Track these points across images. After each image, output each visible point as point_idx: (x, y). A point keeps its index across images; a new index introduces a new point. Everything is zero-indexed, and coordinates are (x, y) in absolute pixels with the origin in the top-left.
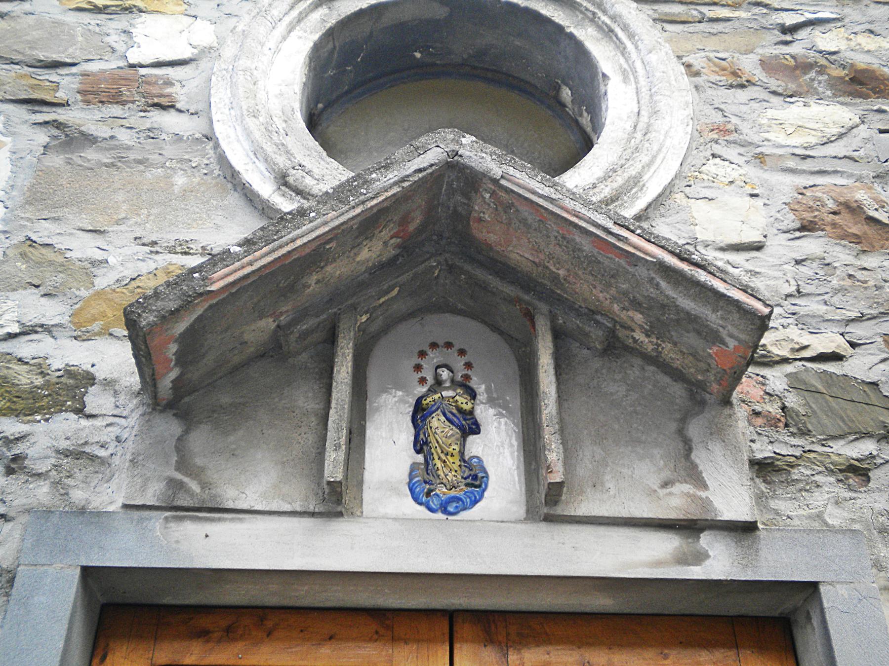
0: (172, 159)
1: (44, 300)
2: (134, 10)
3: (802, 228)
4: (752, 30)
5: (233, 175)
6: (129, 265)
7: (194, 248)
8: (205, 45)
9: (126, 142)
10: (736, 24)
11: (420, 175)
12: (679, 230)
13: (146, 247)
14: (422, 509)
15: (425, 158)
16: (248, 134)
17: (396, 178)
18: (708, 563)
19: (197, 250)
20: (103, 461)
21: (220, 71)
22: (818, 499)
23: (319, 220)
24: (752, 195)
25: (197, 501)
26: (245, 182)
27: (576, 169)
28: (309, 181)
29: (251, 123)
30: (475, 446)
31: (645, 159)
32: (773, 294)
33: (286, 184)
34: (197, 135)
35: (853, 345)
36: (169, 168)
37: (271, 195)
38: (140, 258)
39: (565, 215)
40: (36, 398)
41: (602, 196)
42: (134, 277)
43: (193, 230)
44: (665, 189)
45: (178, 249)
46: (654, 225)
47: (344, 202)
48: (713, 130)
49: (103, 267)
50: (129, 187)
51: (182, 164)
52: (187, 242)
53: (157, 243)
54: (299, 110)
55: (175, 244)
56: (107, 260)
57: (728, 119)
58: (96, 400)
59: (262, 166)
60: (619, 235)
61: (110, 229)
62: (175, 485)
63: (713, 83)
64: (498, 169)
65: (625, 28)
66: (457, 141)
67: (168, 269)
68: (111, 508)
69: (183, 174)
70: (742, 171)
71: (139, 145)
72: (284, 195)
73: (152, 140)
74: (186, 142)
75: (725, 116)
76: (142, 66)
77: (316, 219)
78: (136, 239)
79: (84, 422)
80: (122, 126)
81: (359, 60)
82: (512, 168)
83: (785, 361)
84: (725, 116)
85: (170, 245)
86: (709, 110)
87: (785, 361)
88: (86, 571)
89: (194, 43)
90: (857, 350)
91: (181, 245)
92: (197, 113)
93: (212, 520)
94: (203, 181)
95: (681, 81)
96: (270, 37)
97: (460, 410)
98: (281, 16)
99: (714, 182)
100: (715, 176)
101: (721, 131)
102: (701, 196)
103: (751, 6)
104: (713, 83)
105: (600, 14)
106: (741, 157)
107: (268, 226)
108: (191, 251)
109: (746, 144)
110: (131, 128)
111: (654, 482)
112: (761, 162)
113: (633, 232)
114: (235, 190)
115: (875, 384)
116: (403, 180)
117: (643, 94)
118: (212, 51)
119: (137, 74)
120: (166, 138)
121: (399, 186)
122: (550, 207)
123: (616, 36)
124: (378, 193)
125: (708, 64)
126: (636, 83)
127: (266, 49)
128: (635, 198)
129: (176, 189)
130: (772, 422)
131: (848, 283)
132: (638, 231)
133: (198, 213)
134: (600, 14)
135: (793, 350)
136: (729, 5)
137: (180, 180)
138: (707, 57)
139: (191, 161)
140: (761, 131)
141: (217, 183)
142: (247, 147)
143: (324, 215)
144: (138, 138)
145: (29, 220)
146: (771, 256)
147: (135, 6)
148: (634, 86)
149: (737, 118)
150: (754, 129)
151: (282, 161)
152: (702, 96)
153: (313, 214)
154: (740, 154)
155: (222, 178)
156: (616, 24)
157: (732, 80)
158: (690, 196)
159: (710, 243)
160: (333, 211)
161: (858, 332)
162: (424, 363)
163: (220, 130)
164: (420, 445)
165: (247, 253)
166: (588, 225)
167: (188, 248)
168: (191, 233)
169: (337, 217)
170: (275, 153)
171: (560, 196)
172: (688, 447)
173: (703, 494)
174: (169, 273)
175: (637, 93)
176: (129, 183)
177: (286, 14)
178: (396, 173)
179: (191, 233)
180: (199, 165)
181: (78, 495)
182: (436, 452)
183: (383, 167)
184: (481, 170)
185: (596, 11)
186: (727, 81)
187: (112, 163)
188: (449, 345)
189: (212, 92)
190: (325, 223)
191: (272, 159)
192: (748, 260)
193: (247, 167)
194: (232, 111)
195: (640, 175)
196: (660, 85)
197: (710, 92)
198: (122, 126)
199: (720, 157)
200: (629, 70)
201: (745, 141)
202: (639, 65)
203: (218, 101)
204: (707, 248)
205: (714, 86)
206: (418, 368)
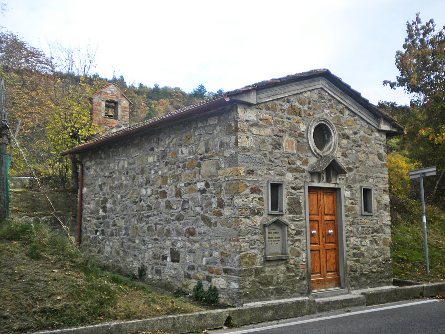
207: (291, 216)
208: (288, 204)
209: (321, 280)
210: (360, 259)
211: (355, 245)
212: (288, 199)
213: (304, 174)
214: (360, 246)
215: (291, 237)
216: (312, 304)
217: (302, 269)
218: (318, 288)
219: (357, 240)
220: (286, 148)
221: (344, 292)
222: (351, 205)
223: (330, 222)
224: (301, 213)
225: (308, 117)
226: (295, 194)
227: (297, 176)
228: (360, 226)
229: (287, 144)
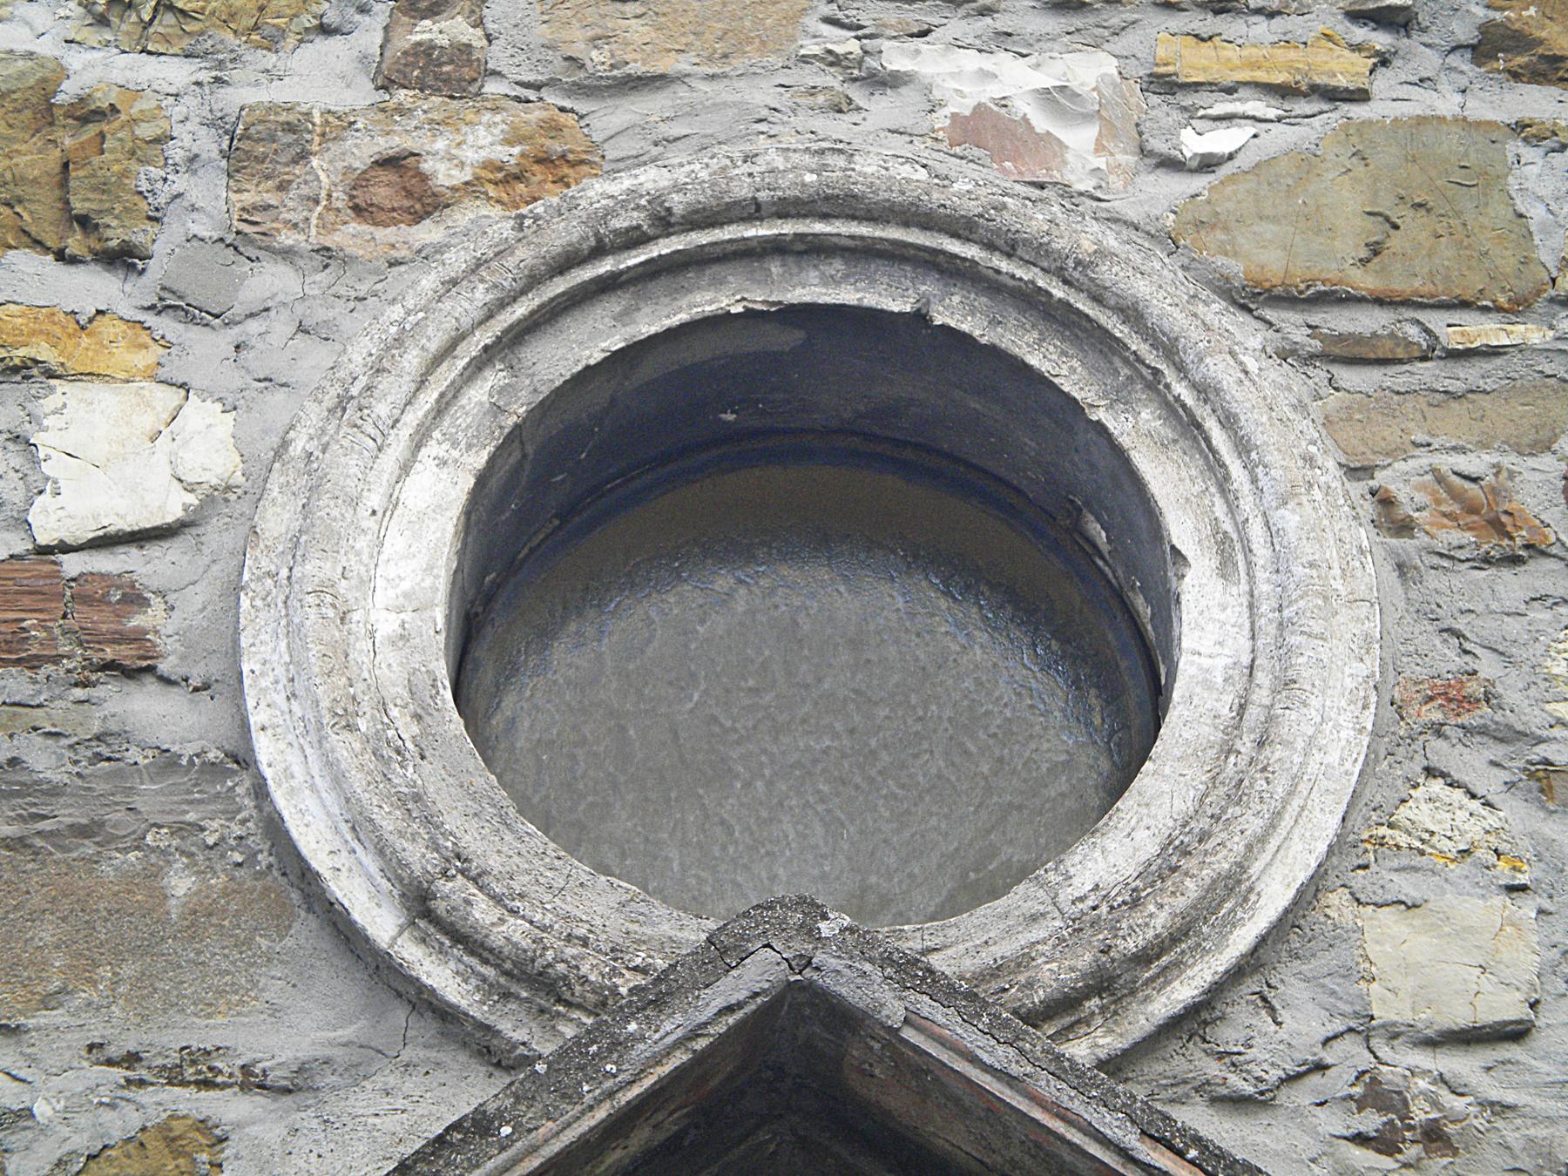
0: (160, 827)
2: (35, 371)
4: (1552, 381)
5: (303, 874)
6: (82, 1120)
7: (226, 1070)
8: (214, 481)
9: (48, 774)
10: (1516, 362)
11: (731, 1021)
12: (1333, 993)
13: (115, 1070)
15: (740, 977)
16: (338, 780)
17: (679, 1033)
19: (231, 1075)
21: (259, 579)
23: (519, 1144)
24: (1512, 889)
26: (333, 900)
27: (1097, 839)
28: (483, 912)
29: (344, 747)
31: (1254, 825)
32: (1540, 1161)
33: (429, 915)
34: (213, 755)
36: (153, 850)
37: (394, 939)
38: (104, 1100)
39: (1037, 1114)
41: (1150, 934)
42: (94, 1151)
43: (219, 1019)
44: (1301, 893)
46: (1273, 982)
47: (570, 1097)
48: (1431, 699)
49: (25, 1128)
50: (65, 905)
51: (183, 838)
52: (209, 1053)
53: (140, 1059)
54: (447, 684)
55: (182, 1059)
56: (30, 1110)
57: (1473, 664)
59: (371, 864)
60: (1150, 1165)
61: (31, 1022)
63: (1441, 555)
64: (896, 1003)
65: (1229, 422)
66: (810, 932)
67: (171, 1130)
69: (187, 866)
70: (1492, 820)
71: (79, 782)
72: (424, 941)
73: (106, 764)
74: (188, 772)
75: (1466, 652)
76: (65, 548)
77: (514, 1141)
78: (91, 1047)
80: (35, 729)
81: (583, 455)
82: (926, 998)
84: (1466, 652)
85: (169, 1062)
86: (1426, 637)
89: (190, 478)
91: (194, 1063)
92: (206, 687)
94: (233, 885)
95: (1359, 573)
96: (371, 477)
98: (397, 412)
99: (1422, 853)
100: (1426, 836)
101: (1450, 700)
102: (1390, 898)
103: (1557, 308)
104: (1441, 555)
105: (1170, 375)
106: (1496, 770)
107: (415, 1162)
108: (219, 1079)
109: (1509, 735)
110: (56, 735)
112: (1542, 791)
113: (1180, 1154)
114: (310, 910)
116: (694, 1035)
117: (1263, 621)
118: (233, 497)
119: (56, 575)
120: (140, 760)
121: (687, 1049)
122: (1007, 1095)
123: (1208, 440)
124: (642, 1071)
125: (1433, 493)
126: (1251, 577)
127: (364, 512)
128: (1232, 923)
132: (1193, 1153)
133: (228, 973)
134: (1170, 375)
136: (1499, 309)
137: (181, 884)
138: (1434, 471)
139: (203, 829)
140: (1548, 696)
141: (267, 889)
142: (336, 810)
143: (530, 1131)
144: (76, 762)
146: (1546, 1057)
147: (36, 362)
148: (1244, 587)
149: (1495, 656)
150: (1533, 691)
151: (418, 857)
152: (1413, 595)
153: (506, 1130)
154: (1494, 764)
155: (276, 873)
156: (1208, 407)
157: (1492, 545)
158: (1363, 899)
159: (1403, 1028)
160: (549, 1119)
163: (265, 749)
166: (1087, 1139)
167: (211, 1069)
168: (215, 1027)
169: (558, 1133)
170: (401, 834)
171: (1029, 1069)
174: (174, 1140)
175: (1251, 606)
176: (66, 896)
177: (409, 403)
178: (678, 1017)
179: (215, 1027)
180: (223, 839)
183: (652, 1002)
184: (861, 1005)
185: (1162, 366)
186: (1478, 547)
187: (21, 839)
189: (244, 642)
190: (533, 1150)
191: (394, 852)
192: (1489, 1069)
193: (339, 861)
194: (295, 705)
195: (1242, 867)
196: (1301, 603)
197: (1433, 581)
198: (35, 729)
199: (1443, 775)
200: (1235, 536)
201: (1509, 727)
202: (1256, 531)
203: (257, 668)
204: (1395, 1042)
205: (1445, 563)
225: (351, 235)
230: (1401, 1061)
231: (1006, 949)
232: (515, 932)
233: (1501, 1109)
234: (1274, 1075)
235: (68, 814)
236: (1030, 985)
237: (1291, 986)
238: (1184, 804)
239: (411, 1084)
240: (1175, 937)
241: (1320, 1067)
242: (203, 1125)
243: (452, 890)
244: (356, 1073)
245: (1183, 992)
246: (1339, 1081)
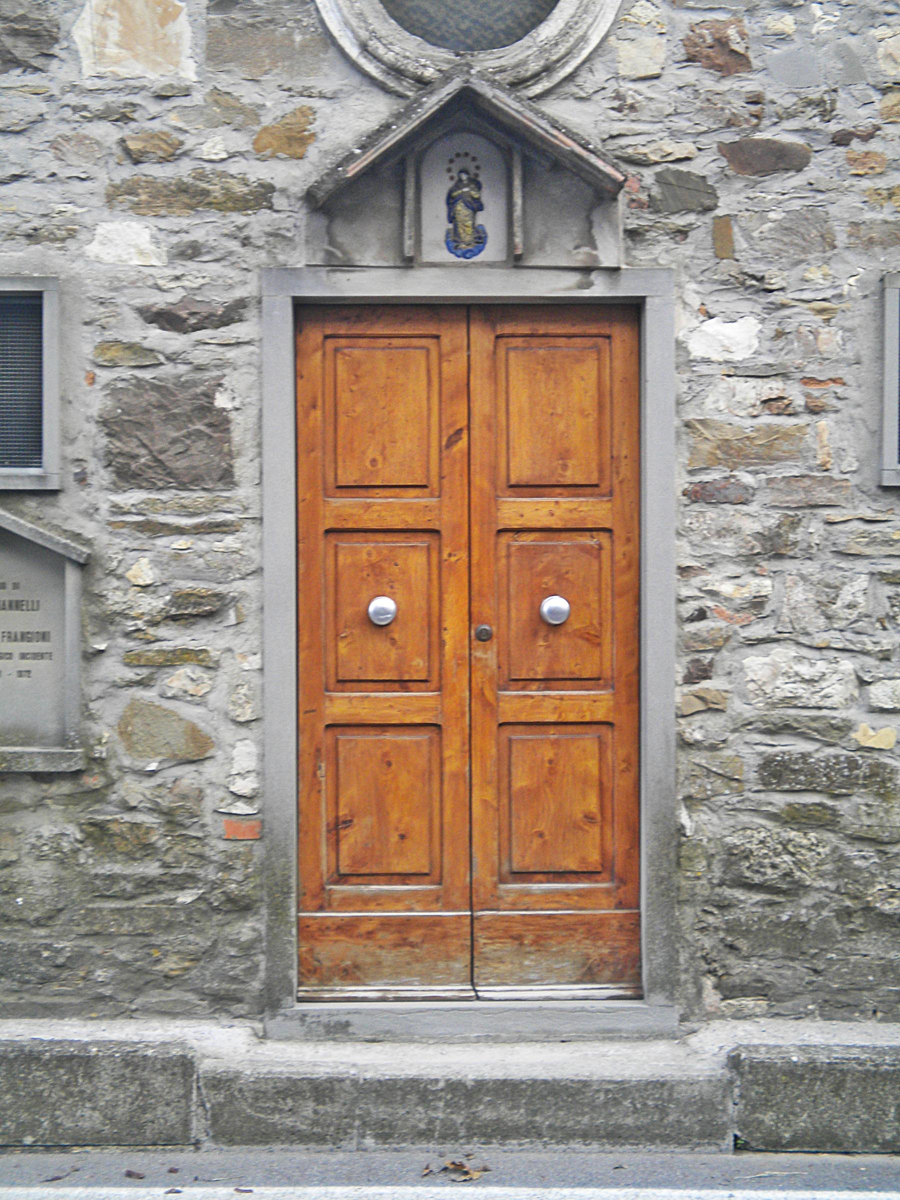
1: (234, 133)
3: (687, 61)
14: (452, 255)
18: (593, 288)
20: (290, 240)
22: (657, 250)
25: (301, 184)
28: (381, 51)
30: (481, 218)
31: (590, 20)
33: (367, 50)
35: (700, 149)
40: (248, 201)
45: (305, 93)
58: (279, 201)
59: (350, 35)
62: (329, 254)
68: (299, 266)
79: (275, 215)
83: (657, 163)
87: (657, 163)
88: (295, 299)
90: (701, 153)
93: (348, 271)
97: (474, 199)
111: (570, 246)
115: (704, 177)
116: (440, 101)
128: (582, 49)
129: (297, 45)
130: (641, 205)
131: (706, 105)
135: (663, 157)
145: (212, 73)
151: (364, 34)
161: (704, 140)
162: (453, 166)
164: (452, 218)
165: (364, 153)
172: (590, 224)
173: (594, 252)
181: (281, 258)
182: (460, 225)
188: (467, 154)
195: (586, 33)
206: (449, 170)
207: (132, 497)
208: (104, 422)
209: (437, 922)
210: (843, 806)
211: (788, 702)
212: (112, 390)
213: (265, 215)
214: (852, 714)
215: (127, 635)
216: (159, 1081)
217: (222, 845)
218: (397, 974)
219: (805, 670)
220: (100, 57)
221: (627, 1025)
222: (766, 419)
223: (565, 541)
224: (227, 477)
226: (172, 358)
227: (198, 236)
228: (861, 566)
229: (114, 28)
230: (626, 87)
231: (521, 57)
232: (390, 57)
233: (650, 99)
234: (591, 91)
235: (265, 16)
236: (526, 71)
237: (598, 65)
238: (572, 11)
239: (364, 97)
240: (567, 54)
241: (604, 89)
242: (310, 108)
243: (373, 44)
244: (350, 94)
245: (568, 69)
246: (609, 93)
